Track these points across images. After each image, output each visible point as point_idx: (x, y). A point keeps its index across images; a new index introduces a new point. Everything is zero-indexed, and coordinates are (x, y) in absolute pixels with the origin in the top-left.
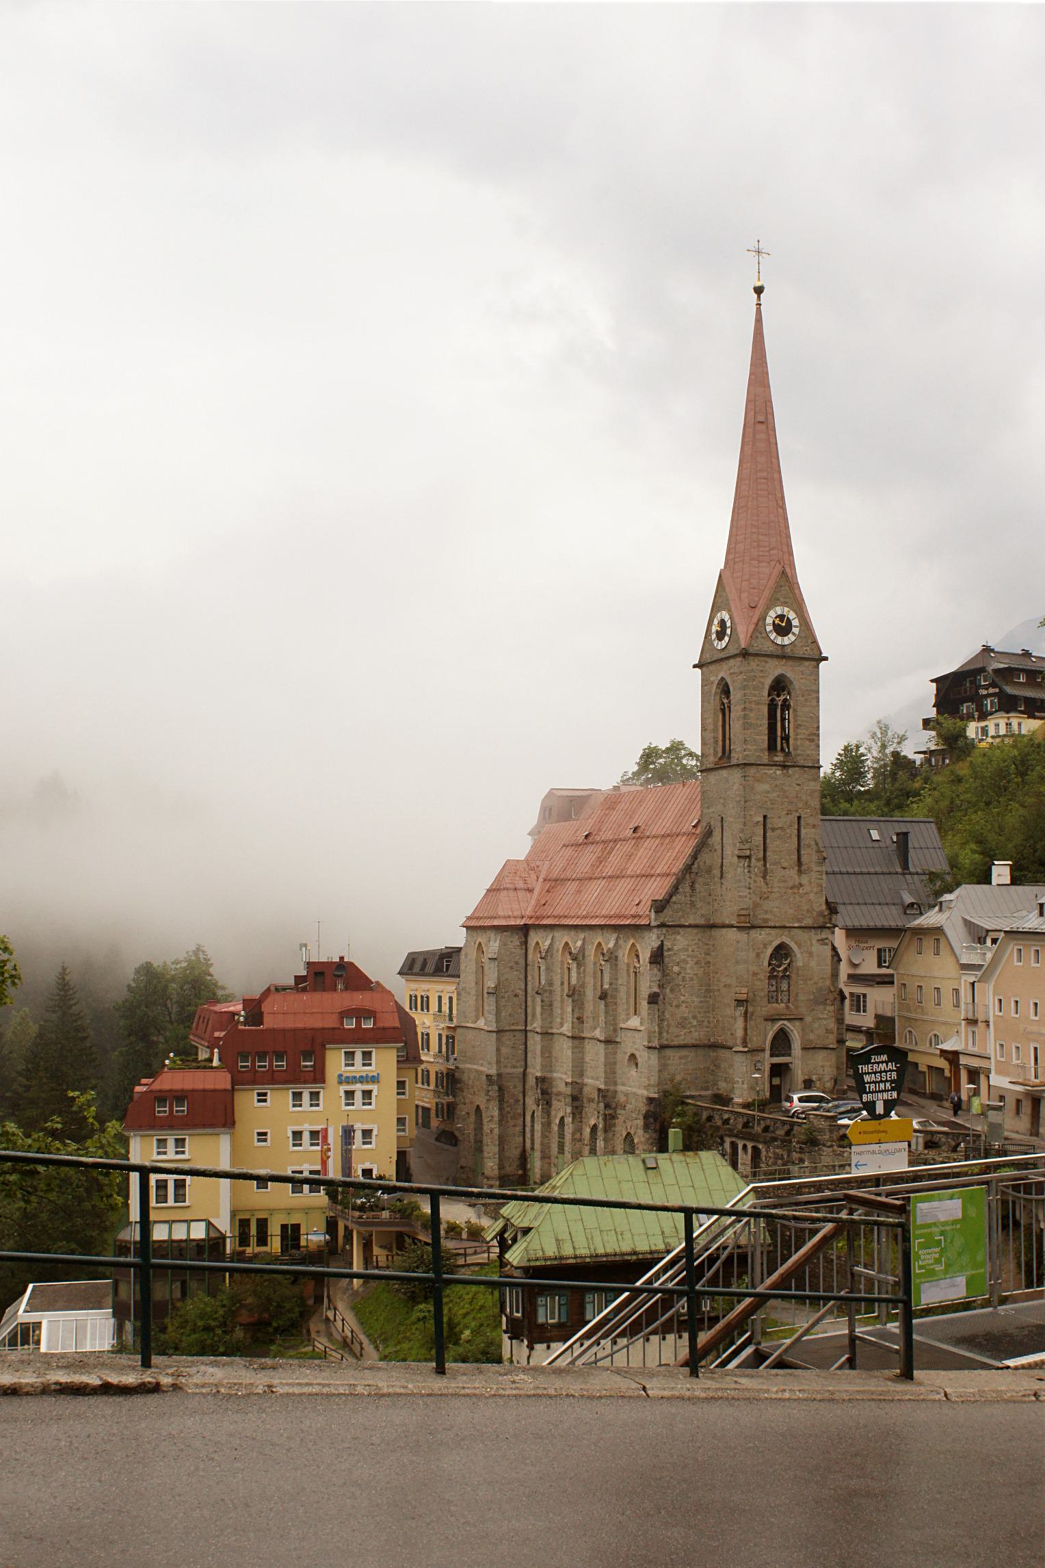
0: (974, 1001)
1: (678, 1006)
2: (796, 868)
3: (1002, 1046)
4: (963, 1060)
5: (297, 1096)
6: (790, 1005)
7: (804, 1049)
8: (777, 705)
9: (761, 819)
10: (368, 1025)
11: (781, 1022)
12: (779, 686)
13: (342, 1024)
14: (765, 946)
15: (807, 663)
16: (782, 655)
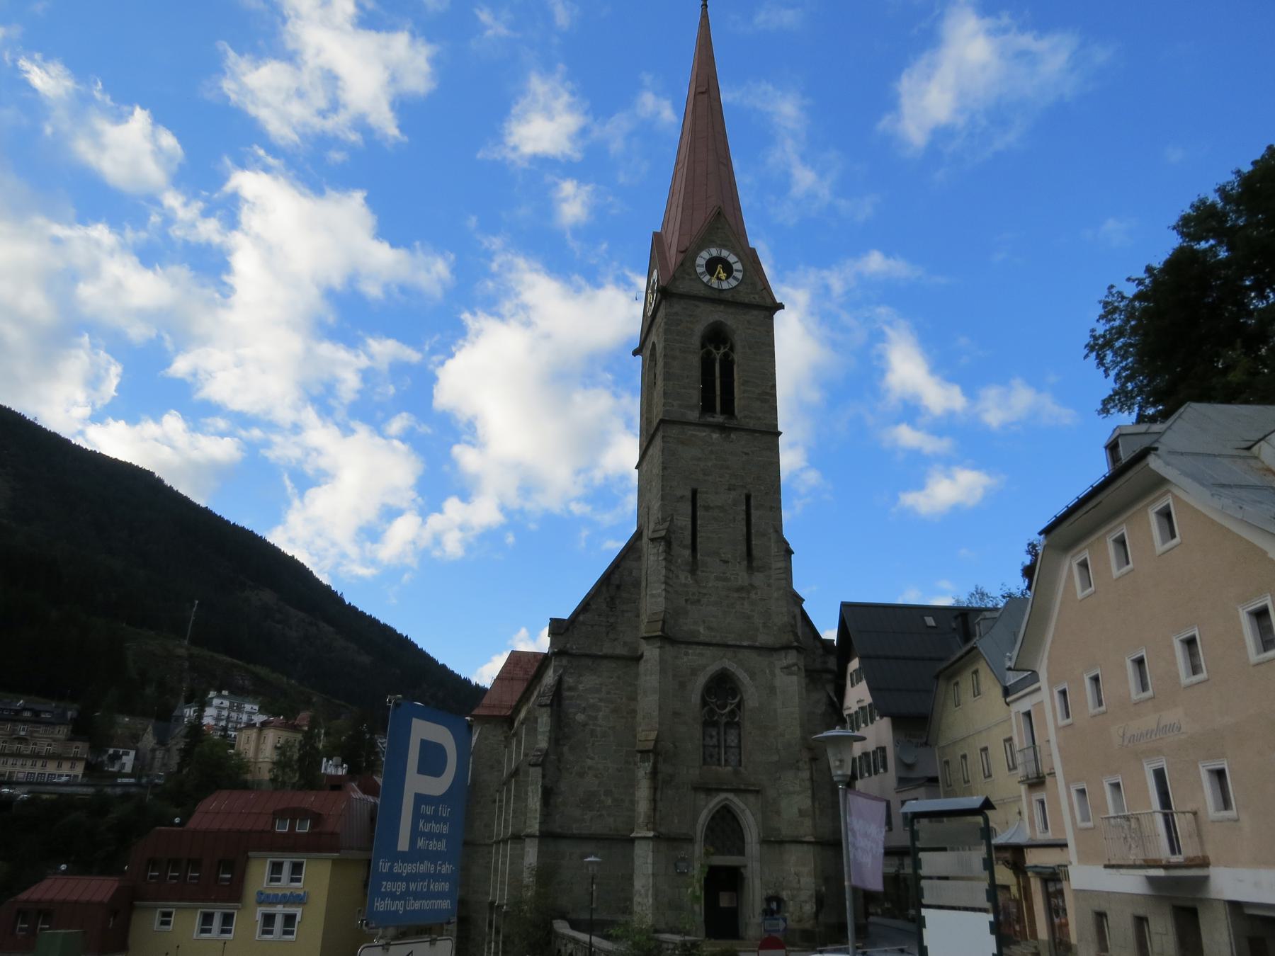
0: (1034, 743)
1: (581, 775)
2: (745, 562)
3: (1082, 792)
4: (1033, 858)
5: (207, 919)
6: (742, 769)
7: (765, 842)
8: (714, 359)
9: (688, 494)
10: (304, 828)
11: (723, 796)
12: (717, 336)
13: (273, 825)
14: (694, 672)
15: (755, 313)
16: (718, 299)
